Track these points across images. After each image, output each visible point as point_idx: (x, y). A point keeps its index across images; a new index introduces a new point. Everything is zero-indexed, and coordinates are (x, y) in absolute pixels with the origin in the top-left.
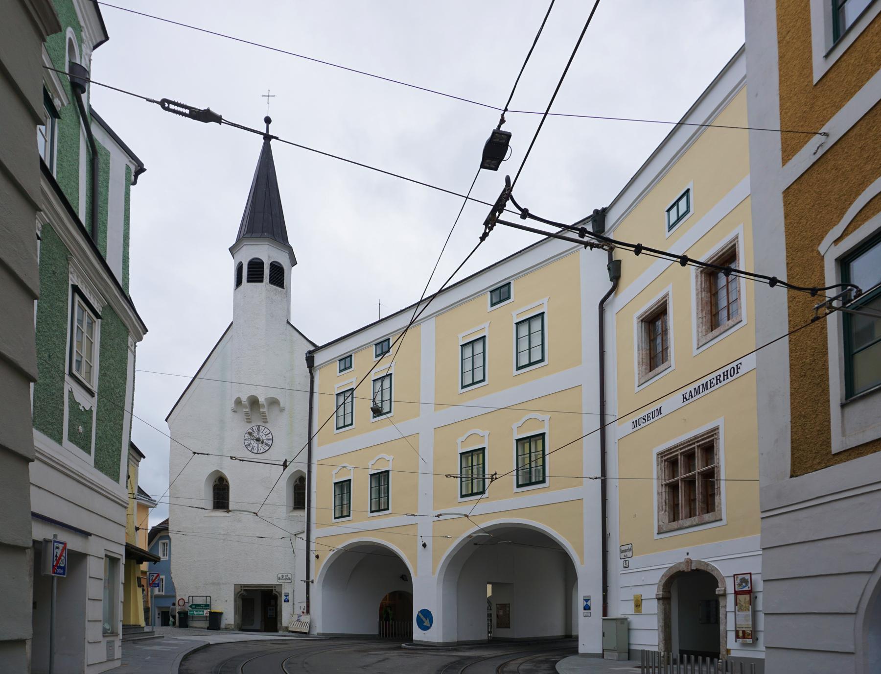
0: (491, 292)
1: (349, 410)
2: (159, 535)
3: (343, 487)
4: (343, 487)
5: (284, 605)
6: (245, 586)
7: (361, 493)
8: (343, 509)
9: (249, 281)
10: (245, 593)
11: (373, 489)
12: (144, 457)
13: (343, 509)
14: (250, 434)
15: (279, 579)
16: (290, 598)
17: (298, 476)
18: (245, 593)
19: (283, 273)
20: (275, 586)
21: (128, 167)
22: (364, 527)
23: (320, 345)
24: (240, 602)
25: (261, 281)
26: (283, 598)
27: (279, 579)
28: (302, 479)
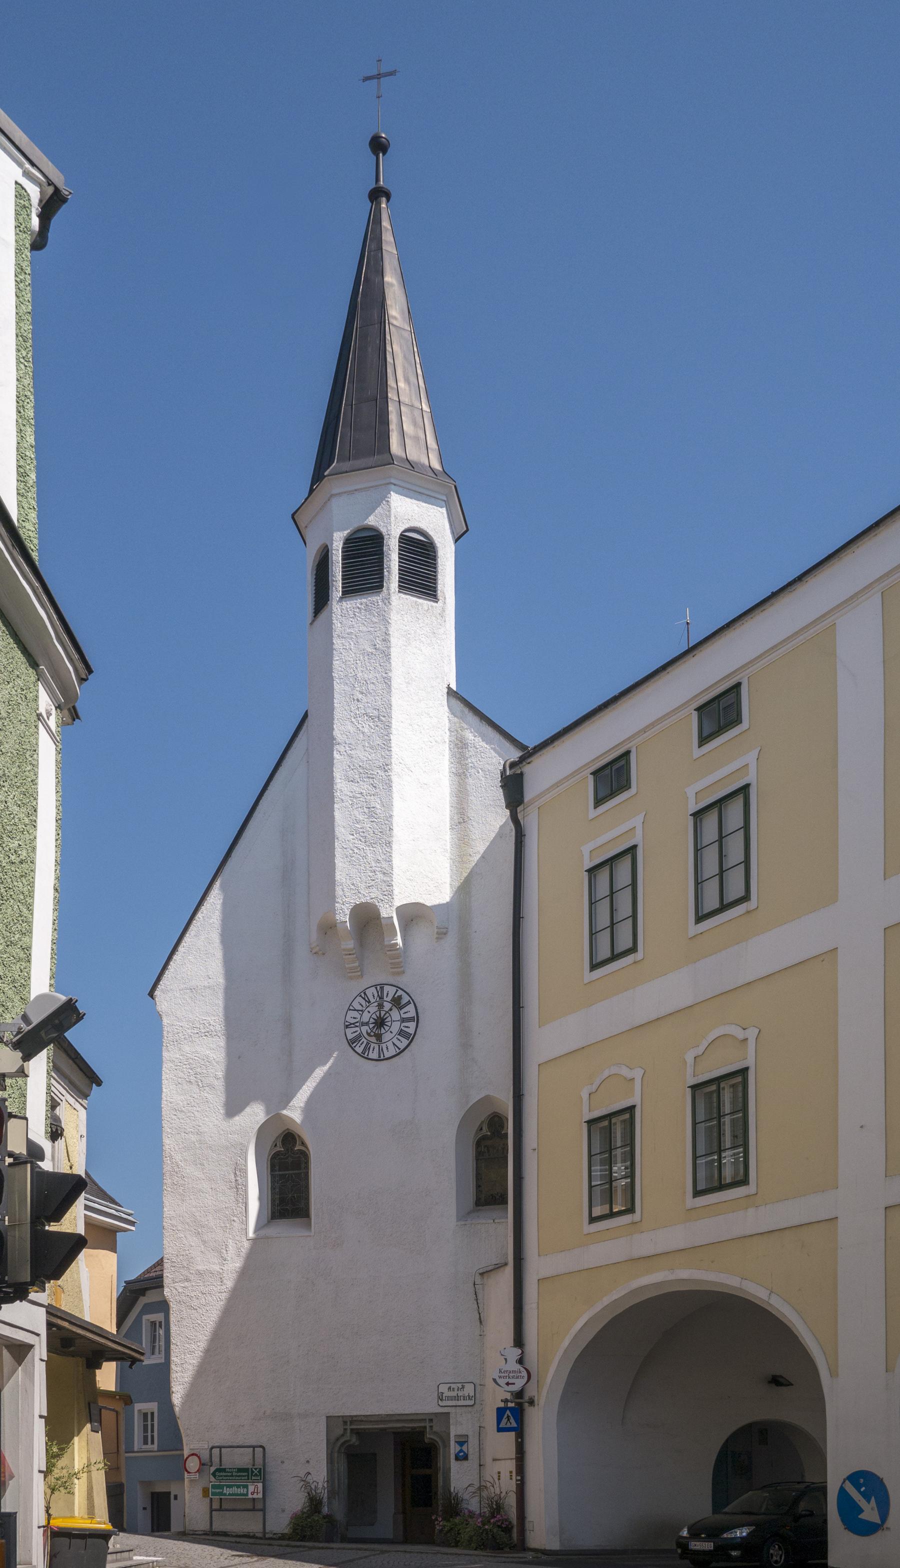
0: (594, 773)
1: (624, 909)
2: (143, 1301)
3: (612, 1135)
4: (612, 1135)
5: (454, 1465)
6: (353, 1420)
7: (665, 1147)
8: (612, 1193)
9: (349, 591)
10: (354, 1440)
11: (701, 1127)
12: (99, 1083)
13: (612, 1193)
14: (397, 1002)
15: (440, 1397)
16: (472, 1448)
17: (484, 1116)
18: (354, 1440)
19: (434, 558)
20: (431, 1418)
21: (20, 193)
22: (674, 1240)
23: (531, 744)
24: (342, 1466)
25: (404, 539)
26: (454, 1448)
27: (440, 1397)
28: (496, 1122)
